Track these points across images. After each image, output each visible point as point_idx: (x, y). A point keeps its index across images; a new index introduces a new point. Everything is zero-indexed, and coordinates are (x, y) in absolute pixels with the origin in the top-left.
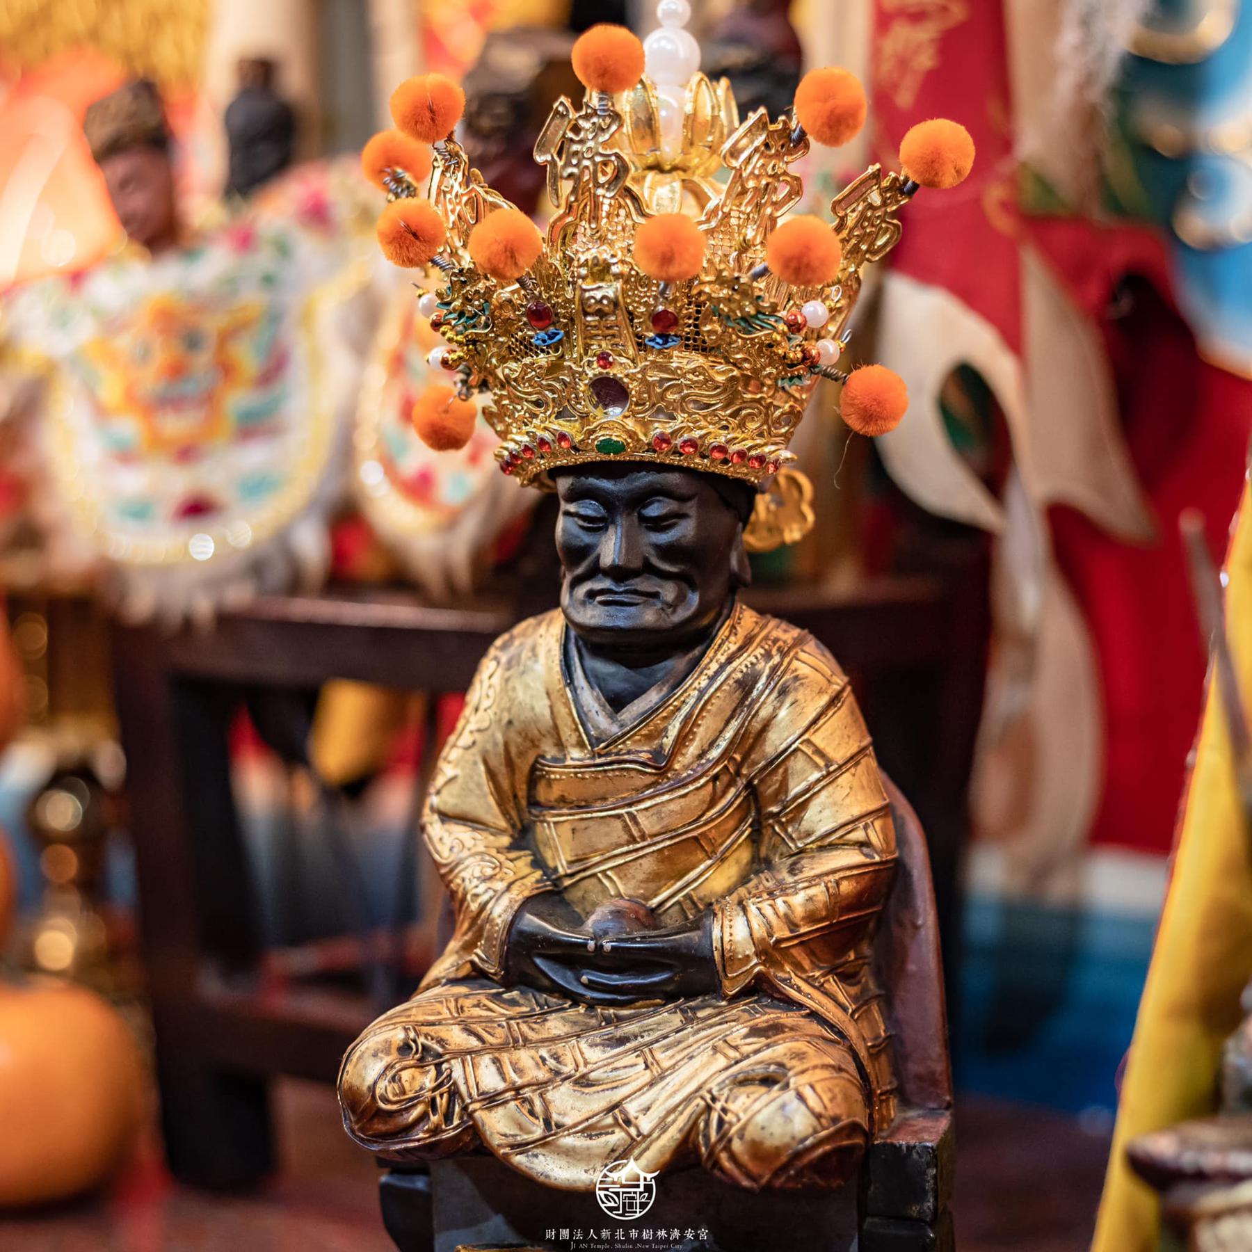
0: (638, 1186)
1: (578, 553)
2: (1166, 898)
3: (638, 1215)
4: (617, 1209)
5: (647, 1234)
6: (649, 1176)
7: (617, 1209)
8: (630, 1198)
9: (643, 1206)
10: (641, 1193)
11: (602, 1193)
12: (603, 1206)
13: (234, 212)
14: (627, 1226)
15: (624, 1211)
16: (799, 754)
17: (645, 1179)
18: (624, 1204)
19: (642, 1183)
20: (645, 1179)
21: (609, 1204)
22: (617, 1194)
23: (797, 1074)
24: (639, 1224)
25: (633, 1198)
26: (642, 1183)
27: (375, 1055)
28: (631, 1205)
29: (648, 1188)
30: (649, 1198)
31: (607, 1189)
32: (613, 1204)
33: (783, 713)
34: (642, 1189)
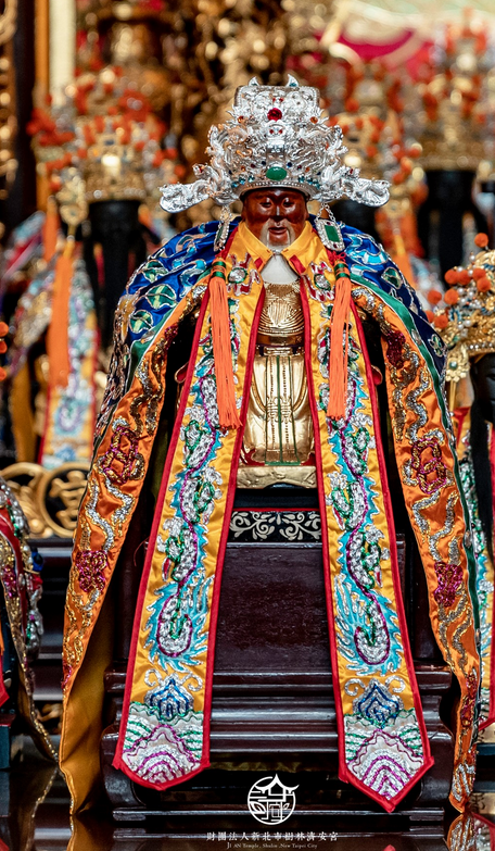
0: (281, 797)
2: (16, 260)
3: (281, 821)
5: (288, 836)
7: (265, 816)
11: (253, 803)
14: (273, 830)
16: (271, 297)
17: (287, 792)
19: (284, 795)
20: (287, 792)
22: (264, 804)
23: (432, 417)
24: (282, 828)
25: (277, 807)
27: (329, 330)
31: (256, 800)
32: (261, 812)
33: (319, 380)
34: (284, 800)
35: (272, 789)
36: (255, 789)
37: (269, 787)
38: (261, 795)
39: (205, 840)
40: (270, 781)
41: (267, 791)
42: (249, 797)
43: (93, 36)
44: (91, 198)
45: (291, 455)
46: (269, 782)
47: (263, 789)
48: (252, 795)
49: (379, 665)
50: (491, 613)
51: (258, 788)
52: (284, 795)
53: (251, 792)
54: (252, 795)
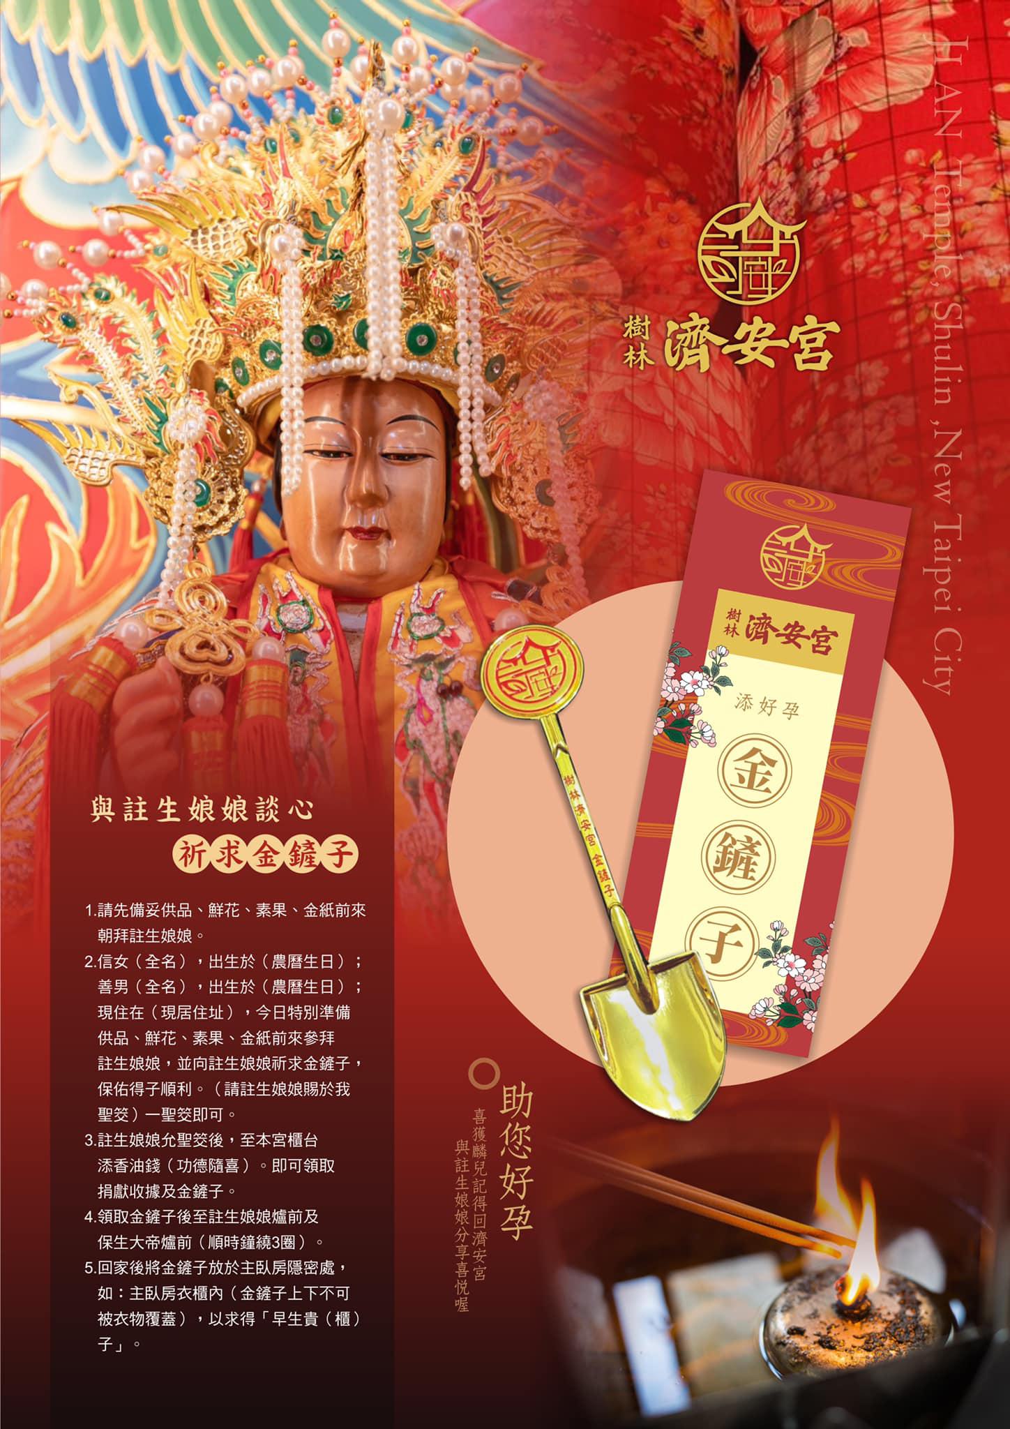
0: (770, 247)
1: (783, 317)
4: (780, 576)
6: (789, 230)
7: (780, 576)
8: (796, 567)
9: (778, 281)
10: (775, 259)
12: (765, 570)
13: (892, 1272)
15: (787, 580)
17: (782, 236)
18: (788, 572)
19: (776, 242)
21: (721, 279)
22: (783, 560)
25: (799, 568)
26: (776, 242)
28: (795, 575)
29: (787, 250)
30: (789, 268)
31: (772, 553)
32: (776, 570)
36: (773, 538)
37: (793, 539)
38: (780, 547)
41: (789, 544)
42: (764, 548)
48: (768, 545)
54: (768, 545)
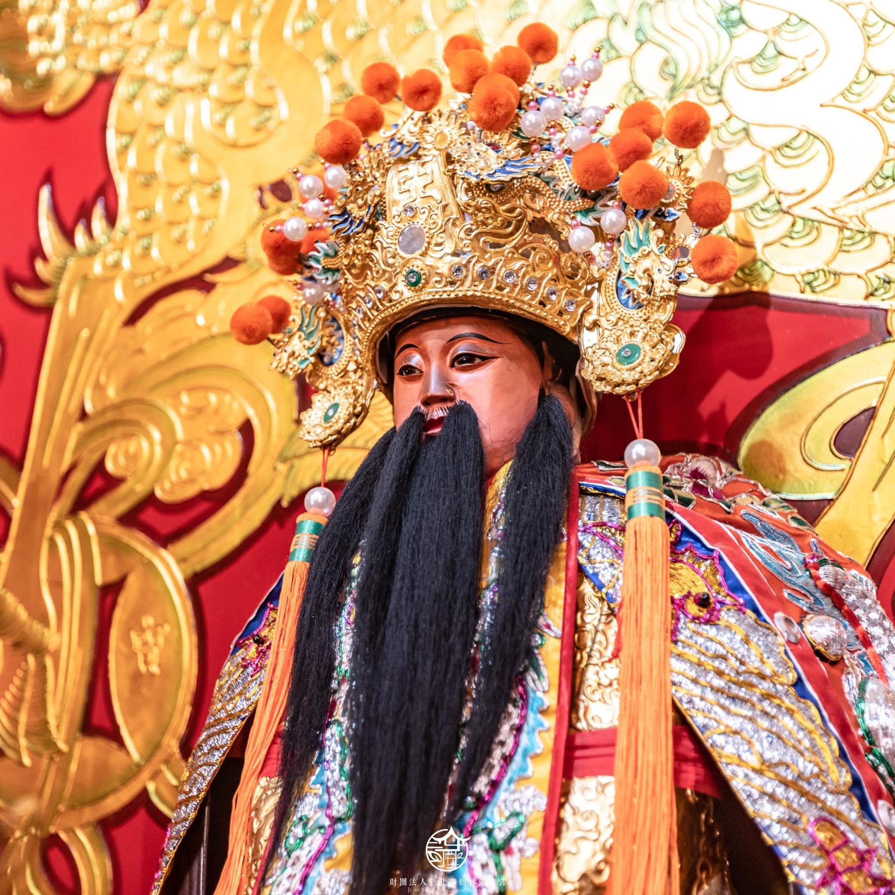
0: (456, 848)
11: (430, 853)
12: (430, 862)
22: (441, 853)
31: (434, 850)
32: (437, 860)
35: (448, 840)
36: (432, 840)
37: (445, 838)
38: (438, 845)
39: (336, 608)
40: (446, 833)
41: (443, 842)
42: (427, 847)
43: (842, 762)
44: (190, 572)
45: (376, 660)
46: (445, 833)
47: (440, 840)
48: (430, 845)
49: (304, 860)
50: (346, 871)
51: (435, 839)
52: (458, 845)
53: (429, 842)
54: (430, 845)
